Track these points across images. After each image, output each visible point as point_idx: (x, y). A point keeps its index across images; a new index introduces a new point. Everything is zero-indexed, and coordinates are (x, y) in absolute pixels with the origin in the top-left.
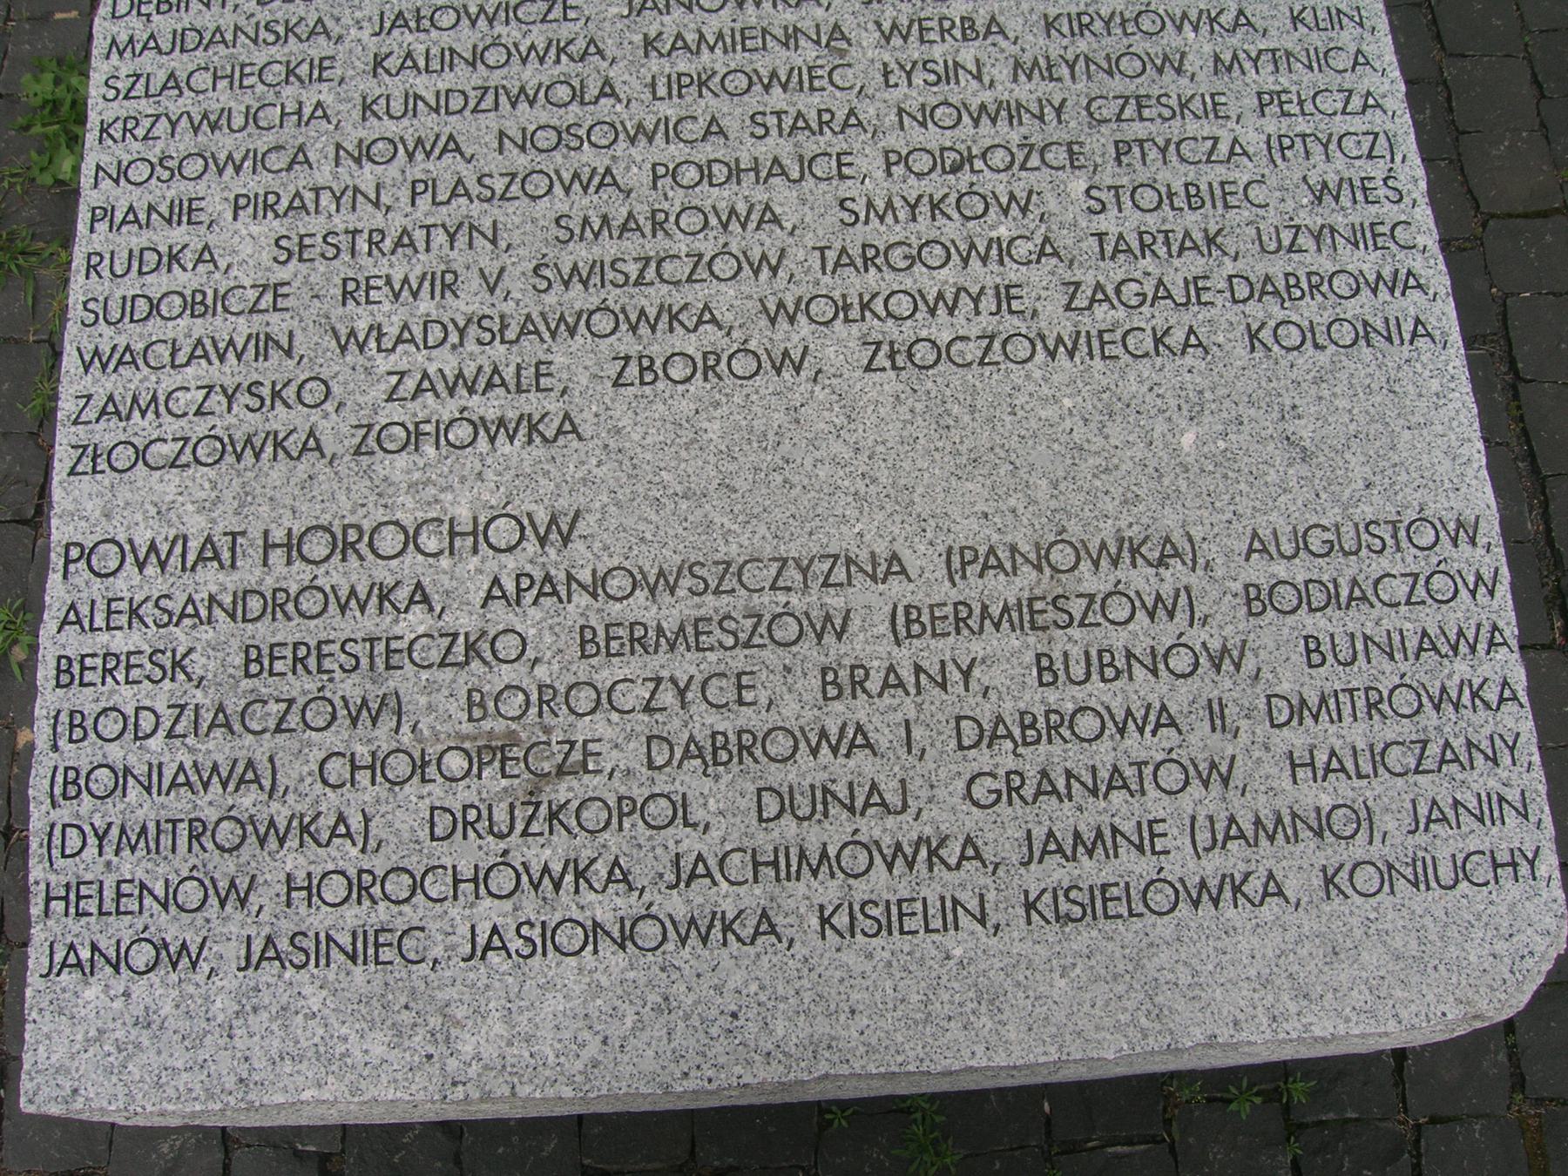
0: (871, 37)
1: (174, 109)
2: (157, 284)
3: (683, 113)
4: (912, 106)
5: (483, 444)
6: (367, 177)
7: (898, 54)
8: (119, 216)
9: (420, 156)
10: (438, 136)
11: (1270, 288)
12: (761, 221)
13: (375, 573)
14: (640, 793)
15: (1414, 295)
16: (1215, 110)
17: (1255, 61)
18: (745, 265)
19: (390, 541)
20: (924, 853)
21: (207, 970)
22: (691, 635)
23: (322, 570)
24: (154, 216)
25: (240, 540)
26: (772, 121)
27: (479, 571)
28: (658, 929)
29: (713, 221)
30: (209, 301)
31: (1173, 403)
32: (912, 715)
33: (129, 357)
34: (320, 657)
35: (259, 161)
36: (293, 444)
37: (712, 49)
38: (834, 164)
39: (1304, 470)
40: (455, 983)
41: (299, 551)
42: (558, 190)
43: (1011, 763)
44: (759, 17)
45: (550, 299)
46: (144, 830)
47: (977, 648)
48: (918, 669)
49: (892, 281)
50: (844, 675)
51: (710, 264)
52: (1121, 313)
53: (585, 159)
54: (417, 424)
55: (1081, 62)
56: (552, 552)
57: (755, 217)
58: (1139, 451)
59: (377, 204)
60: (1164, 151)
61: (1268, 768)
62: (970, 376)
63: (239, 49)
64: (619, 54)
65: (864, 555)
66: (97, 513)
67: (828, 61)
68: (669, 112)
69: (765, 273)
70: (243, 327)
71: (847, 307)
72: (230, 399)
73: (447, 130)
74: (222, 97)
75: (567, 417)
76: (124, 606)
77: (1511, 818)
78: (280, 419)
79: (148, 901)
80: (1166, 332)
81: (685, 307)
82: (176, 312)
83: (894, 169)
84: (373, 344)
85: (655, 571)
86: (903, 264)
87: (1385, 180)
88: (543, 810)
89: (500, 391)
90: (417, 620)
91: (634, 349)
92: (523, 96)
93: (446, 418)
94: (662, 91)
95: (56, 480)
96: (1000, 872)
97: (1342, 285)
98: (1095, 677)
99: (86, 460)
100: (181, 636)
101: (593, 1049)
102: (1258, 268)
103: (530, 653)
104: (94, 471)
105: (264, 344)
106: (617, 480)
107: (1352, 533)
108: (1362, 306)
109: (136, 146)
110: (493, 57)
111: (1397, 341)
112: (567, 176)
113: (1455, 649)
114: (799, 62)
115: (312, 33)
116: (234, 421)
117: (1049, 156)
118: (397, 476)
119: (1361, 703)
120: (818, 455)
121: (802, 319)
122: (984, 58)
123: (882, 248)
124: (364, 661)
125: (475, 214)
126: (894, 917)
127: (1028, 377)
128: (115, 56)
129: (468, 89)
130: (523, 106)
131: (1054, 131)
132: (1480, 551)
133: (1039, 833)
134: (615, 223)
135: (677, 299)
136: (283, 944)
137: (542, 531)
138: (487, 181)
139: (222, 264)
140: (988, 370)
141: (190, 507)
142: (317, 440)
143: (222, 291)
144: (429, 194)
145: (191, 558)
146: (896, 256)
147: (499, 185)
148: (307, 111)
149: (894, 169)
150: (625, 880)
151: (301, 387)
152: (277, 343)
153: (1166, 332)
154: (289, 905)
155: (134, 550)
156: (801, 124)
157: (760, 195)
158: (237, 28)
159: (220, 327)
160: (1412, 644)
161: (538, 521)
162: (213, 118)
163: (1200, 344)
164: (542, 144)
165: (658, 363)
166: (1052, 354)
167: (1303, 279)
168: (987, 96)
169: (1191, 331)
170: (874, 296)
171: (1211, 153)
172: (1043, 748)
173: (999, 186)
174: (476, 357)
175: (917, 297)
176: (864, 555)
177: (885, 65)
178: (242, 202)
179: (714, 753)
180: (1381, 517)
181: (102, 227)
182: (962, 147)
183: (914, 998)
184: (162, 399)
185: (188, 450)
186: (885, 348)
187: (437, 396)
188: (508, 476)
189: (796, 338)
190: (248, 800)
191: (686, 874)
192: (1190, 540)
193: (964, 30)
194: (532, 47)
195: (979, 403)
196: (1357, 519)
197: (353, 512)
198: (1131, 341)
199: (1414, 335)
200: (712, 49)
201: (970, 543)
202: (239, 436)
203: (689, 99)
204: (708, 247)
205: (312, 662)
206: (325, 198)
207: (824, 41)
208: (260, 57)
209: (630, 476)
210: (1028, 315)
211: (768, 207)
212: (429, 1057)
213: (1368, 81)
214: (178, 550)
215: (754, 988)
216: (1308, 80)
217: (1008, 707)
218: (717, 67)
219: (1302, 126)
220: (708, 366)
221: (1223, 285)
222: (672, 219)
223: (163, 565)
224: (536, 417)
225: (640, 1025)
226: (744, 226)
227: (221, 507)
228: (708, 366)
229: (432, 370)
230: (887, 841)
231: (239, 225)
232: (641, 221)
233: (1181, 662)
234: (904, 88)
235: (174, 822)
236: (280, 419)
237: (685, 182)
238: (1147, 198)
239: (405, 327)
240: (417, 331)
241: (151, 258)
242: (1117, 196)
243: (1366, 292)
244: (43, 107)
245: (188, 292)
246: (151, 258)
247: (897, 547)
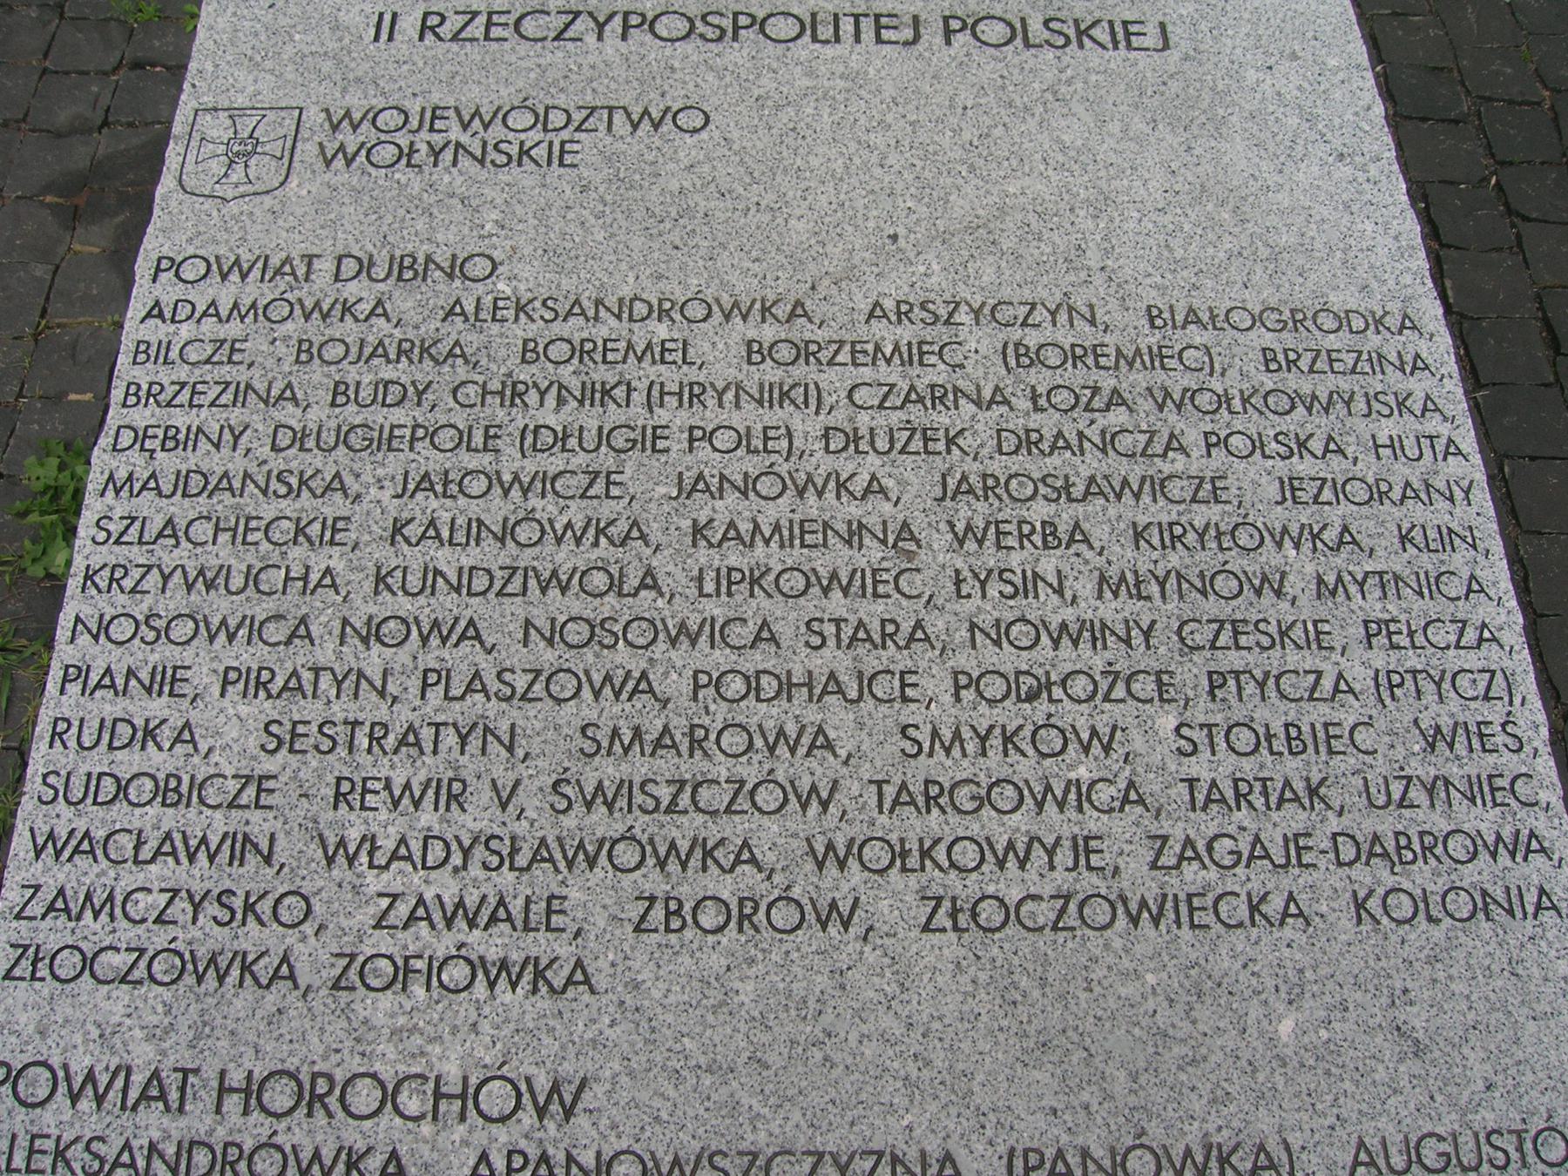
0: (945, 539)
1: (168, 560)
2: (128, 762)
3: (732, 614)
4: (985, 621)
5: (480, 989)
6: (374, 660)
7: (972, 560)
8: (94, 678)
9: (435, 641)
10: (456, 620)
11: (1378, 849)
12: (812, 746)
13: (344, 1135)
15: (1538, 860)
16: (1317, 640)
17: (1362, 584)
18: (792, 797)
19: (364, 1097)
23: (283, 1125)
24: (133, 682)
25: (191, 1079)
26: (829, 629)
27: (465, 1143)
29: (759, 743)
30: (184, 789)
31: (1270, 983)
33: (87, 846)
35: (256, 630)
36: (263, 969)
37: (767, 542)
38: (897, 683)
41: (259, 1099)
42: (586, 693)
44: (821, 509)
45: (569, 821)
49: (958, 825)
51: (752, 792)
52: (1213, 874)
53: (618, 660)
54: (407, 959)
55: (1173, 580)
56: (551, 1126)
57: (806, 740)
58: (1230, 1040)
59: (382, 693)
60: (1262, 685)
62: (1043, 942)
63: (246, 499)
64: (664, 540)
65: (912, 1154)
66: (31, 1028)
67: (894, 564)
68: (716, 612)
69: (814, 808)
70: (220, 823)
71: (905, 854)
72: (196, 908)
73: (468, 613)
74: (223, 552)
75: (579, 964)
76: (49, 1145)
78: (252, 937)
80: (1263, 899)
81: (722, 842)
82: (146, 797)
83: (963, 693)
84: (364, 859)
85: (669, 1158)
86: (969, 806)
87: (1503, 725)
89: (504, 927)
91: (661, 888)
92: (553, 581)
93: (441, 954)
94: (709, 587)
97: (1457, 846)
99: (25, 963)
102: (1369, 825)
104: (33, 978)
105: (241, 846)
106: (632, 1045)
107: (1472, 1145)
108: (1479, 872)
109: (122, 599)
110: (525, 533)
111: (1519, 915)
112: (597, 678)
114: (863, 563)
115: (328, 488)
116: (199, 934)
117: (1136, 687)
118: (379, 1019)
120: (864, 1028)
121: (853, 864)
122: (1066, 569)
123: (947, 785)
125: (491, 714)
127: (1107, 946)
128: (110, 494)
129: (494, 567)
130: (554, 592)
131: (1141, 658)
134: (648, 737)
135: (713, 833)
137: (541, 1100)
138: (507, 676)
139: (203, 746)
140: (1062, 936)
141: (138, 1033)
142: (291, 967)
143: (200, 778)
144: (441, 688)
145: (133, 1094)
147: (521, 682)
148: (314, 577)
149: (963, 693)
151: (278, 901)
152: (255, 846)
153: (1263, 899)
155: (68, 1078)
156: (861, 635)
157: (812, 715)
158: (246, 475)
159: (193, 820)
161: (538, 1089)
162: (209, 575)
163: (1301, 914)
164: (572, 639)
165: (687, 908)
166: (1135, 920)
167: (1415, 840)
168: (1068, 614)
169: (1291, 898)
170: (937, 842)
171: (1313, 689)
173: (1079, 718)
174: (480, 884)
175: (985, 846)
176: (912, 1154)
177: (957, 572)
178: (233, 675)
180: (1505, 1125)
181: (74, 689)
182: (1039, 672)
184: (119, 899)
185: (143, 964)
186: (947, 904)
187: (433, 926)
188: (506, 1031)
189: (845, 887)
192: (1288, 1148)
193: (1045, 536)
194: (569, 525)
195: (1051, 976)
196: (1476, 1126)
197: (325, 1058)
198: (1223, 908)
199: (1539, 907)
200: (767, 542)
201: (1035, 1144)
202: (203, 952)
203: (739, 598)
204: (750, 772)
205: (355, 799)
206: (326, 681)
207: (891, 541)
208: (268, 510)
209: (647, 1041)
210: (1108, 872)
211: (820, 730)
213: (1482, 611)
214: (119, 1083)
216: (1420, 608)
218: (772, 563)
219: (1413, 661)
220: (744, 914)
221: (1326, 844)
222: (713, 737)
223: (100, 1099)
224: (543, 962)
226: (793, 751)
227: (174, 1037)
228: (744, 914)
229: (429, 895)
231: (226, 702)
232: (678, 738)
234: (977, 600)
236: (252, 937)
237: (729, 695)
238: (1244, 739)
239: (403, 841)
240: (416, 846)
241: (124, 731)
242: (1210, 736)
243: (1484, 856)
244: (43, 493)
245: (161, 776)
246: (124, 731)
247: (952, 1145)
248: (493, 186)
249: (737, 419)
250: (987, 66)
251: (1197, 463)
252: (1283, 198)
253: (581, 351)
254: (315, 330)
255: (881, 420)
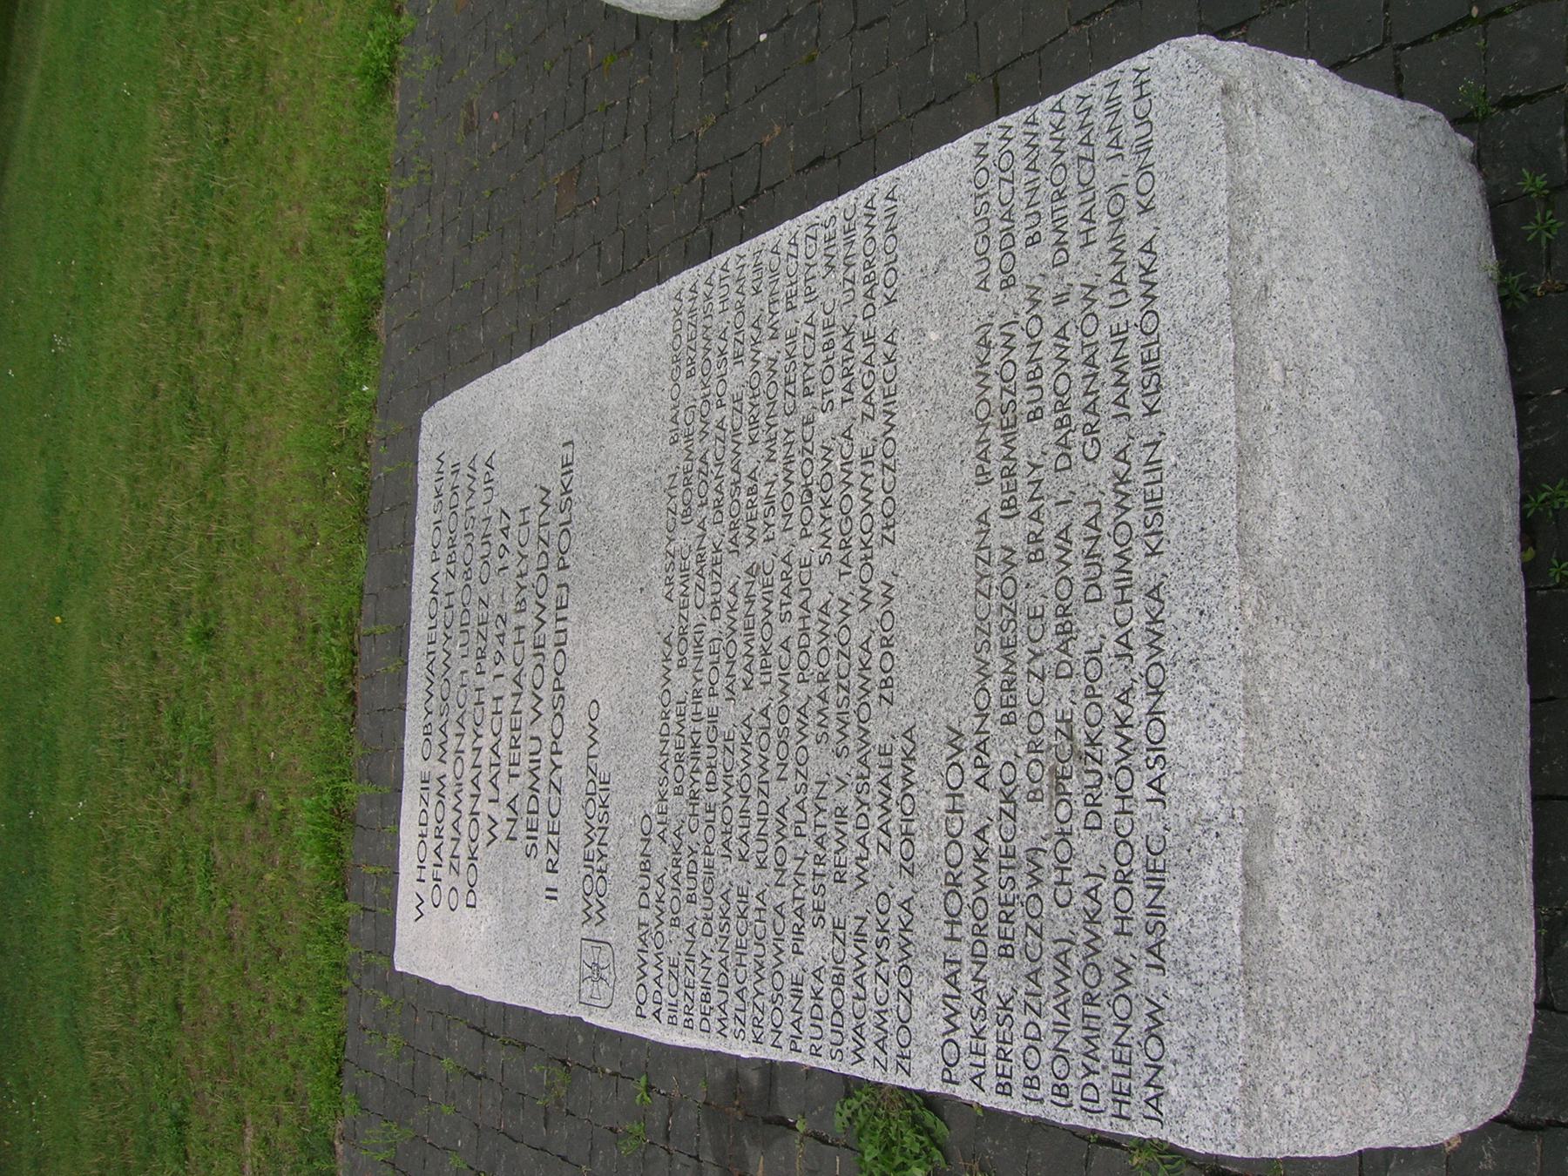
1: (752, 993)
2: (828, 1009)
14: (1085, 683)
19: (954, 854)
20: (1121, 487)
21: (1163, 999)
22: (1008, 647)
28: (1153, 669)
32: (1052, 501)
34: (1007, 904)
39: (950, 260)
40: (1178, 814)
43: (1079, 433)
45: (852, 746)
46: (1087, 1039)
47: (1023, 461)
48: (1032, 499)
50: (1032, 548)
52: (876, 385)
56: (966, 744)
61: (1088, 262)
65: (977, 539)
67: (761, 575)
72: (883, 960)
77: (1118, 92)
79: (1124, 1040)
84: (864, 863)
88: (1089, 750)
90: (992, 835)
91: (877, 692)
93: (900, 815)
95: (911, 1086)
96: (1132, 434)
98: (1039, 382)
100: (993, 1002)
101: (1216, 714)
103: (1012, 759)
105: (860, 936)
113: (1035, 147)
118: (924, 848)
119: (1059, 204)
124: (1011, 873)
126: (1154, 505)
132: (991, 140)
133: (1115, 410)
136: (1152, 940)
139: (822, 963)
146: (845, 528)
150: (1126, 692)
154: (1130, 934)
159: (850, 965)
160: (1032, 176)
172: (1072, 413)
179: (1067, 633)
183: (1196, 486)
190: (1075, 961)
191: (1126, 652)
206: (799, 894)
212: (1217, 835)
215: (1187, 600)
217: (1052, 438)
219: (801, 283)
220: (887, 643)
225: (1204, 680)
228: (887, 643)
230: (1114, 513)
233: (1035, 325)
234: (774, 528)
235: (1085, 1016)
248: (616, 820)
249: (706, 671)
250: (578, 544)
251: (727, 412)
252: (631, 371)
253: (679, 761)
254: (666, 918)
255: (709, 590)
